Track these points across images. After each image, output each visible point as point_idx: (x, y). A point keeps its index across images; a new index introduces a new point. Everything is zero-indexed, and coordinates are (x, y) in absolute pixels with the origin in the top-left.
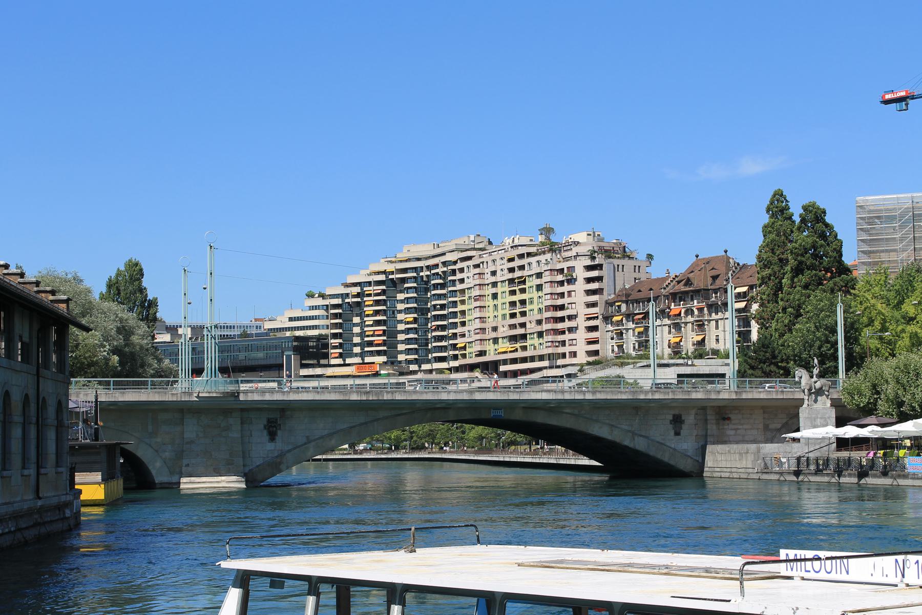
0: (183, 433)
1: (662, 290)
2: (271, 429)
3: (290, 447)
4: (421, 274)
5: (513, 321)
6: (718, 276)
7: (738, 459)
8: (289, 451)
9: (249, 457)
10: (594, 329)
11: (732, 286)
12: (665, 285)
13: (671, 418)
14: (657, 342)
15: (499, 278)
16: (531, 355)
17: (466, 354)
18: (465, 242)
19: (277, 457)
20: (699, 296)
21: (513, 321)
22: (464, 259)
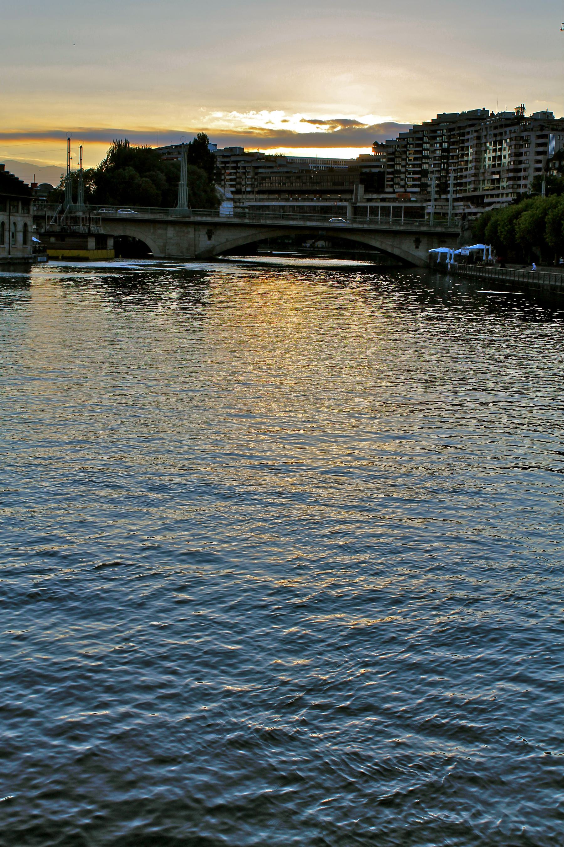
0: (167, 234)
3: (218, 244)
8: (217, 245)
14: (15, 223)
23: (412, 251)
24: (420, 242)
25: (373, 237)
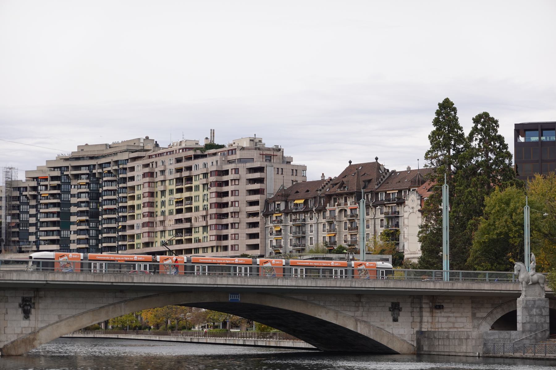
1: (319, 192)
2: (26, 308)
4: (94, 171)
5: (179, 216)
6: (370, 181)
7: (457, 344)
8: (42, 329)
9: (5, 333)
10: (255, 225)
11: (446, 186)
12: (321, 187)
13: (390, 306)
15: (168, 176)
16: (195, 247)
17: (134, 244)
18: (135, 144)
19: (30, 334)
20: (352, 198)
21: (179, 216)
22: (134, 159)
23: (388, 326)
24: (400, 310)
25: (322, 304)
